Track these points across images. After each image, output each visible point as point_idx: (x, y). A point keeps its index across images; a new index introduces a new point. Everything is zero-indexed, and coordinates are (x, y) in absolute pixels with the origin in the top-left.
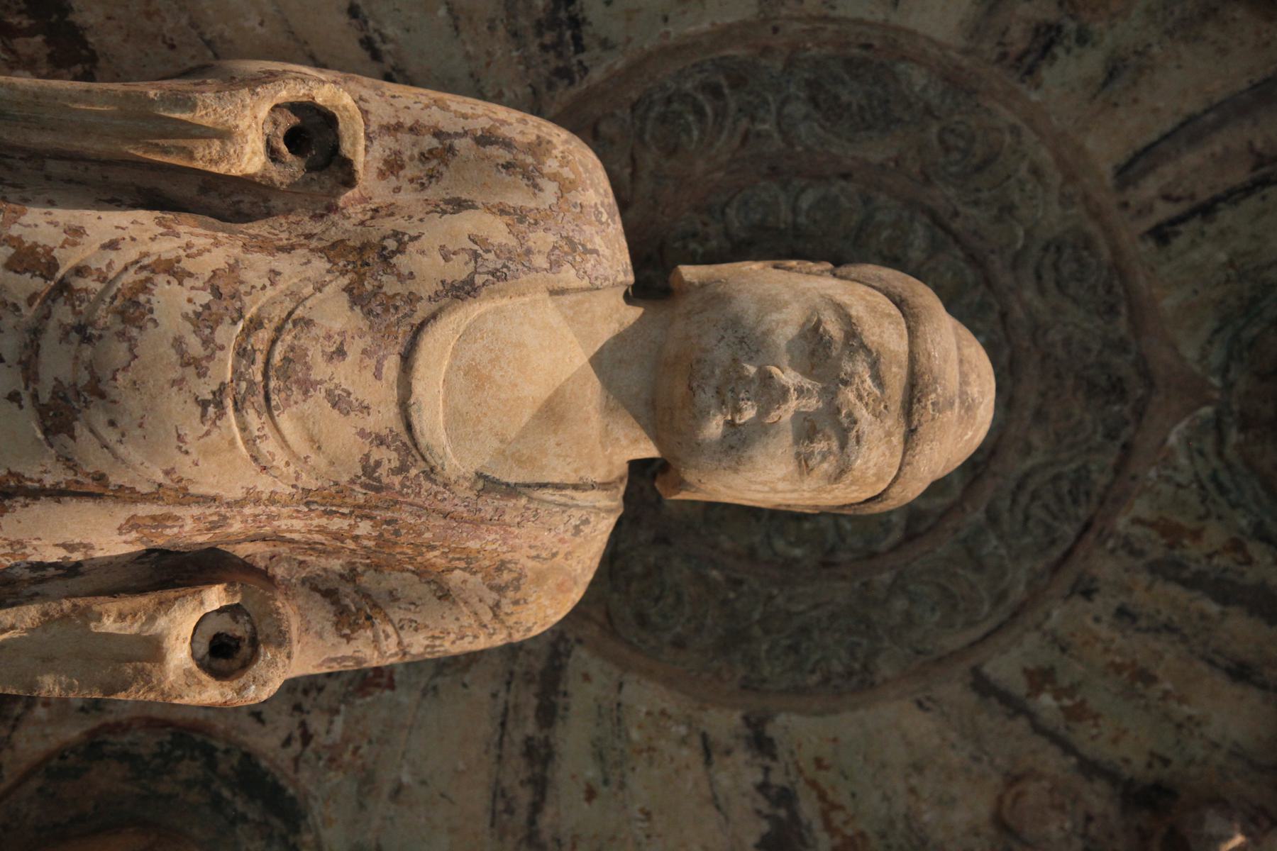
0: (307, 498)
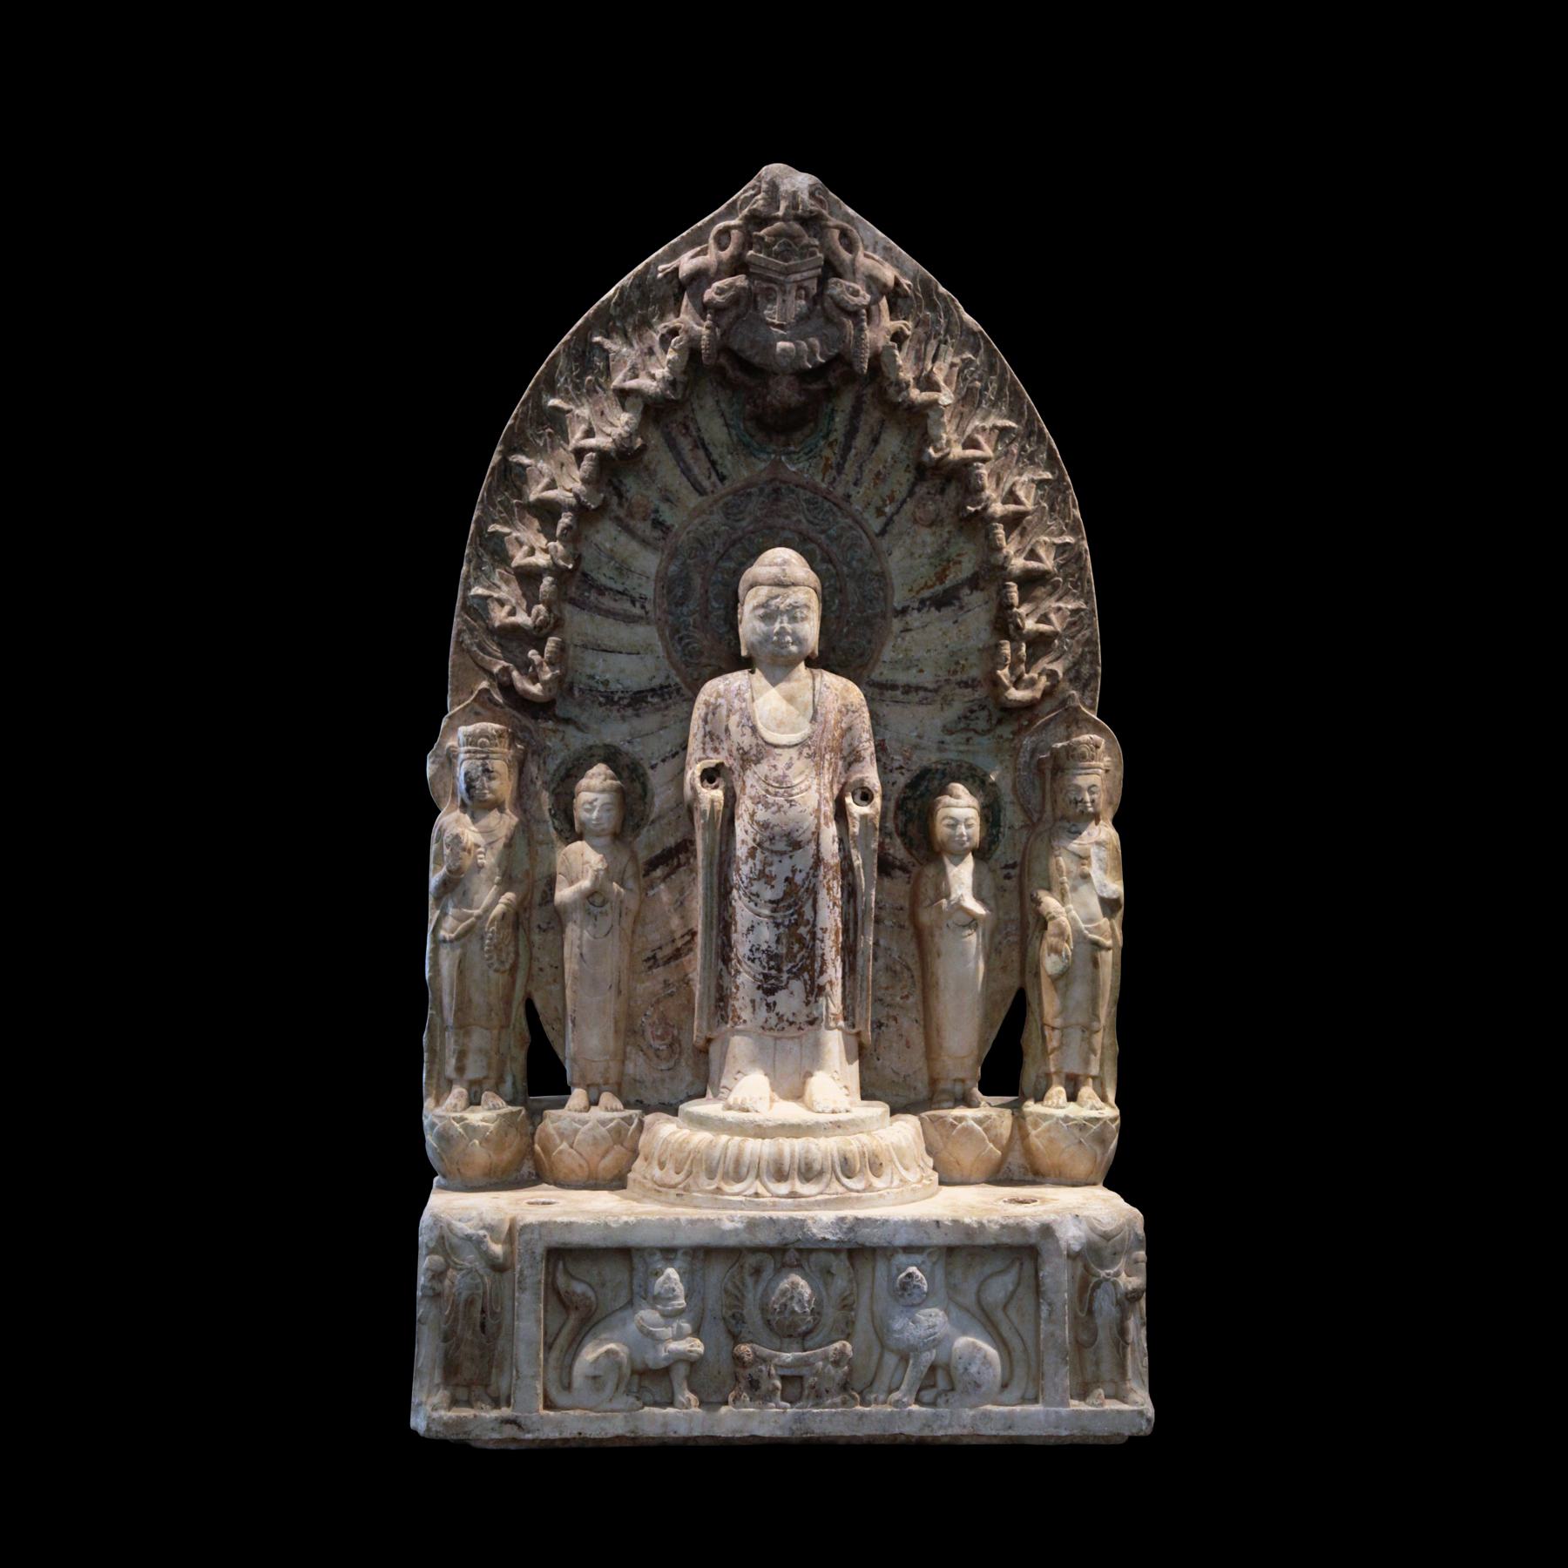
0: (819, 774)
